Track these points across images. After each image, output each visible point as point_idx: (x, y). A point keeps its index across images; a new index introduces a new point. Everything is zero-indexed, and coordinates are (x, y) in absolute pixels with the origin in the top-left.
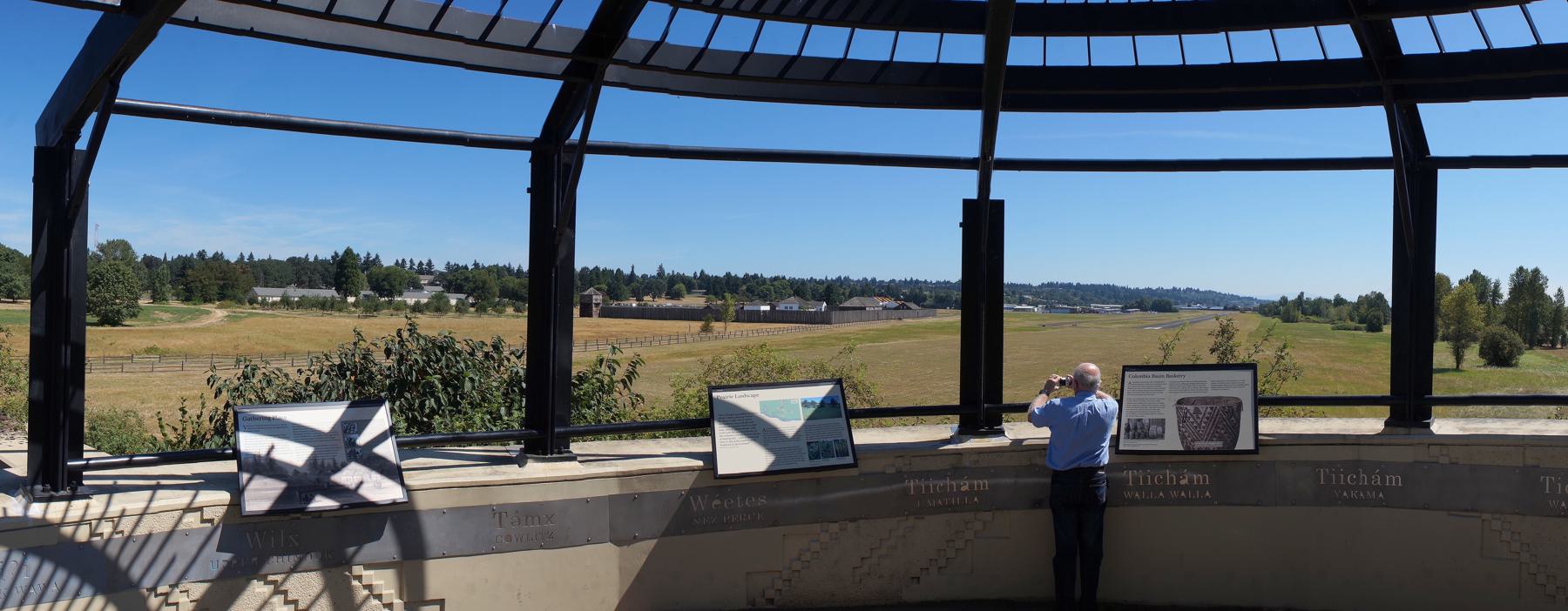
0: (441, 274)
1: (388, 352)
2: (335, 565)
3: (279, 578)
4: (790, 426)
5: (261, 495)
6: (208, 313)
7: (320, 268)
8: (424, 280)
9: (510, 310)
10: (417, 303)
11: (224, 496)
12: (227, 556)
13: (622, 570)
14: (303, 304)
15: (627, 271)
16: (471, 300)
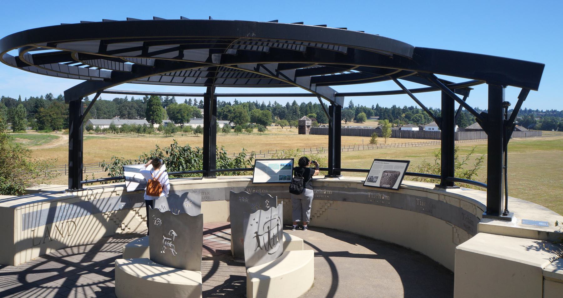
1: (167, 152)
3: (137, 209)
4: (277, 171)
5: (132, 187)
6: (57, 138)
7: (135, 105)
9: (255, 130)
11: (122, 188)
12: (124, 203)
14: (124, 130)
16: (232, 124)
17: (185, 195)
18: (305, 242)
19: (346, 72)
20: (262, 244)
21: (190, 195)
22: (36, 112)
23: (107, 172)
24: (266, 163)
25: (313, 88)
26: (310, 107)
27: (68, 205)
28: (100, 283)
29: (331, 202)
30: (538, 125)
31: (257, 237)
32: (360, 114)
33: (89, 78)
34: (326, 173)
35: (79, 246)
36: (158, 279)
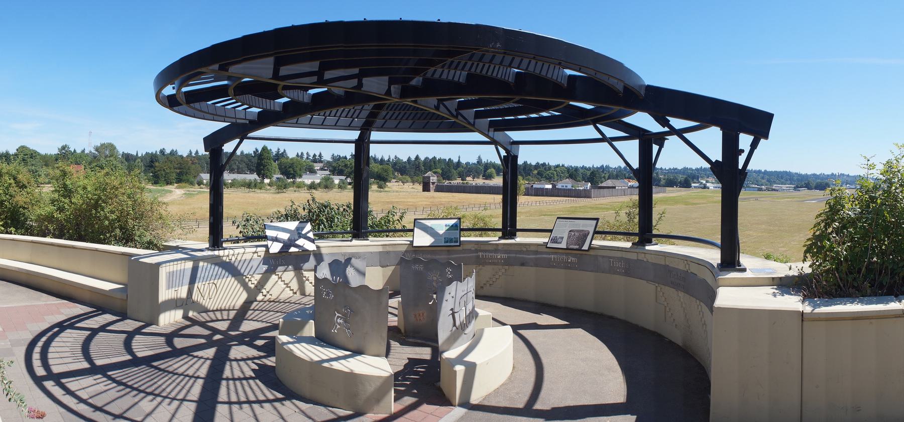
0: (328, 162)
1: (304, 209)
2: (298, 269)
3: (280, 274)
4: (441, 232)
5: (275, 248)
6: (170, 192)
7: (245, 159)
8: (317, 166)
10: (313, 183)
11: (264, 249)
13: (383, 276)
15: (455, 160)
16: (349, 180)
17: (348, 261)
18: (493, 319)
19: (545, 114)
20: (458, 323)
21: (354, 261)
22: (151, 166)
23: (239, 229)
24: (429, 223)
25: (491, 134)
26: (435, 162)
27: (209, 265)
28: (255, 358)
29: (507, 267)
30: (663, 182)
31: (453, 314)
32: (489, 171)
33: (234, 120)
34: (500, 234)
35: (221, 310)
36: (336, 365)
